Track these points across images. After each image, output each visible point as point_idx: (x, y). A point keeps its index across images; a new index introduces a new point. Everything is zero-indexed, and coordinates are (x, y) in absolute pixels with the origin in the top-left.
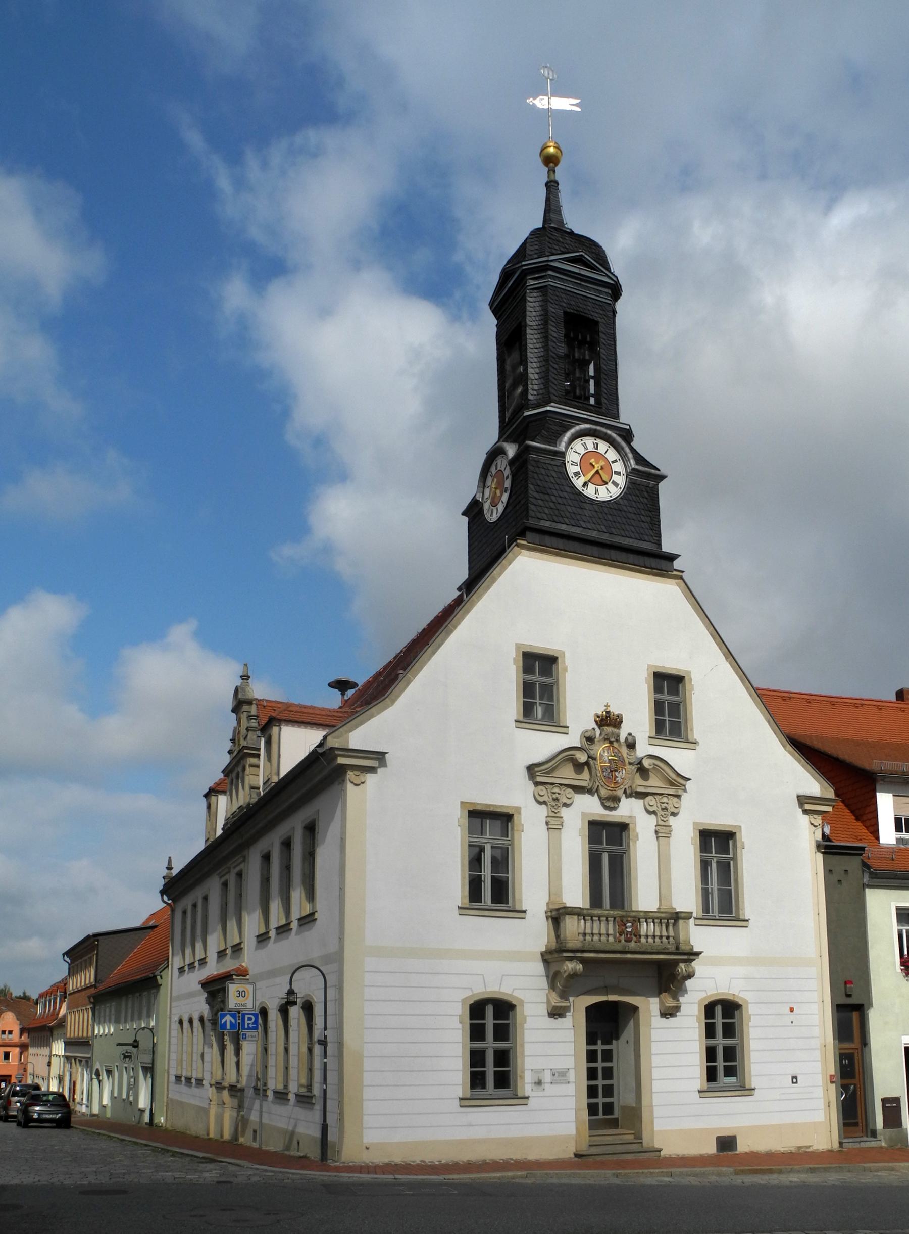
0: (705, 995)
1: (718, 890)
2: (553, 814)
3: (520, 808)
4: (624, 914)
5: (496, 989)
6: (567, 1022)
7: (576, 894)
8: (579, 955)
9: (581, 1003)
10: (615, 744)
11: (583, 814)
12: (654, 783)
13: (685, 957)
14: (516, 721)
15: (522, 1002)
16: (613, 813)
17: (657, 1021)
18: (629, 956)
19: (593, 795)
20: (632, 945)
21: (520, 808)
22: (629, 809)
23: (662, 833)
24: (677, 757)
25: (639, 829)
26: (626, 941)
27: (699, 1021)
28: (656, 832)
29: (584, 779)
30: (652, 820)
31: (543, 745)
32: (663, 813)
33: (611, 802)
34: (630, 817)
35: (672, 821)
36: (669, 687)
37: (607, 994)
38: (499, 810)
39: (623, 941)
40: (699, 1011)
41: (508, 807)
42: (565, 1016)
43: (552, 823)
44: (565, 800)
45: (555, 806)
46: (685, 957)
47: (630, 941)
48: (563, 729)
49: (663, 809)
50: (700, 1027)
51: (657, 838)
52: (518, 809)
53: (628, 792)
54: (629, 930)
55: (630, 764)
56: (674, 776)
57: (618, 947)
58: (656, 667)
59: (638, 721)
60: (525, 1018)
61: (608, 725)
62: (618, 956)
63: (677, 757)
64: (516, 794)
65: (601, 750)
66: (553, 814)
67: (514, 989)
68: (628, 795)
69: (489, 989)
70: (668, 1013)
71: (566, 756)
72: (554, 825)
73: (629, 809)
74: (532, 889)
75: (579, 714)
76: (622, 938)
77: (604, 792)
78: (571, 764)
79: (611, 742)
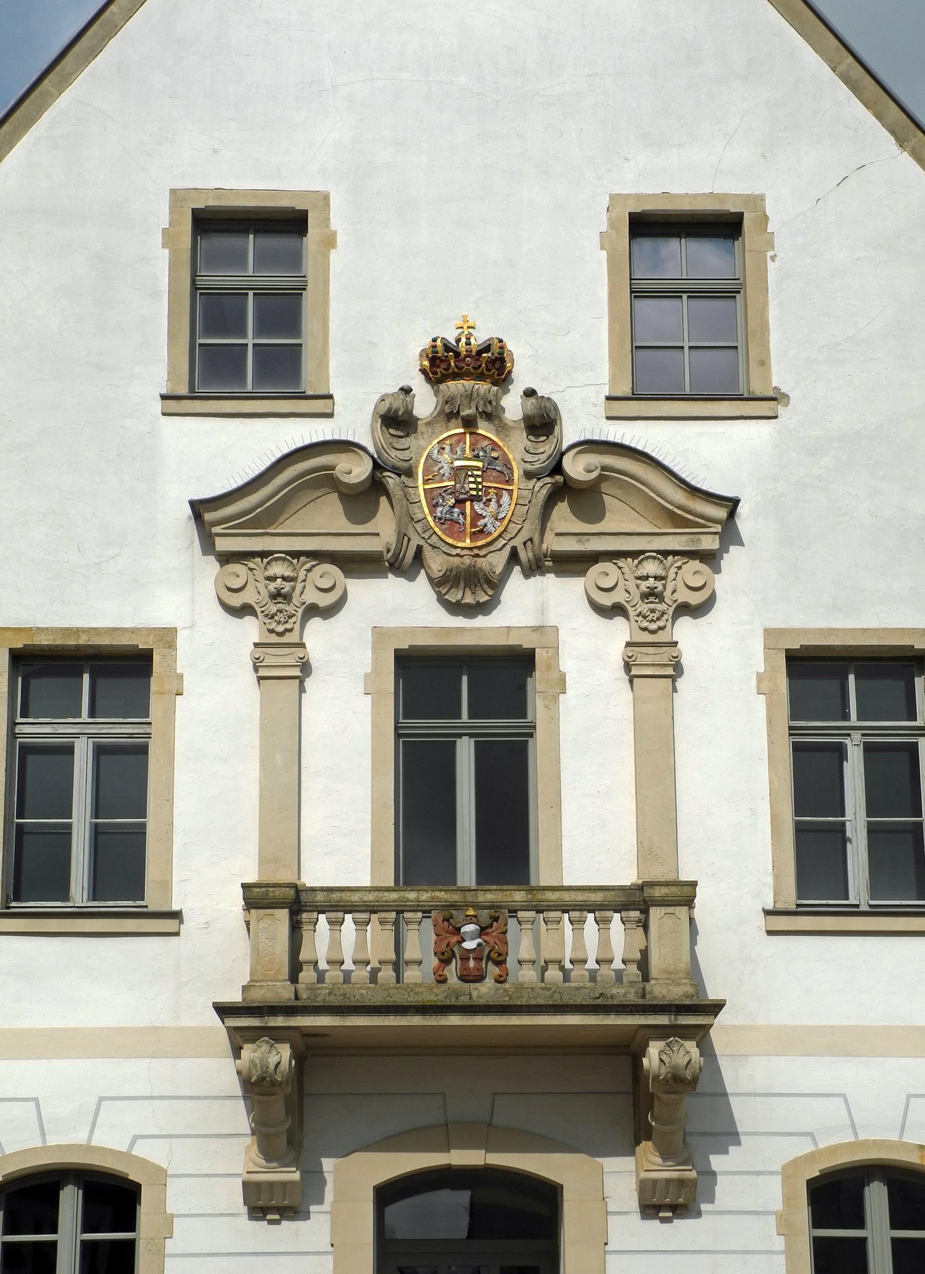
0: (809, 1148)
1: (872, 830)
2: (274, 639)
3: (173, 631)
4: (456, 897)
5: (79, 1137)
6: (314, 1230)
7: (346, 836)
8: (279, 1021)
9: (353, 1179)
10: (484, 429)
11: (379, 634)
12: (621, 520)
13: (663, 1020)
14: (164, 397)
15: (160, 1175)
16: (480, 621)
17: (629, 1229)
18: (455, 1020)
19: (411, 577)
20: (485, 990)
21: (173, 631)
22: (525, 606)
23: (654, 668)
24: (701, 449)
25: (568, 664)
26: (464, 978)
27: (784, 1225)
28: (628, 667)
29: (382, 532)
30: (619, 631)
31: (241, 446)
32: (644, 608)
33: (470, 588)
34: (538, 629)
35: (685, 631)
36: (685, 251)
37: (446, 1147)
38: (105, 641)
39: (453, 980)
40: (787, 1199)
41: (133, 631)
42: (306, 1216)
43: (269, 661)
44: (312, 597)
45: (281, 618)
46: (663, 1020)
47: (480, 978)
48: (322, 404)
49: (645, 596)
50: (789, 1252)
51: (631, 682)
52: (168, 636)
53: (524, 555)
54: (470, 945)
55: (529, 475)
56: (679, 496)
57: (438, 996)
58: (639, 197)
59: (570, 359)
60: (169, 1221)
61: (456, 376)
62: (417, 1020)
63: (701, 449)
64: (163, 593)
65: (436, 452)
66: (274, 639)
67: (135, 1138)
68: (534, 568)
69: (52, 1141)
70: (669, 1202)
71: (305, 473)
72: (284, 671)
73: (525, 606)
74: (204, 849)
75: (366, 353)
76: (452, 971)
77: (437, 563)
78: (335, 496)
79: (469, 423)
